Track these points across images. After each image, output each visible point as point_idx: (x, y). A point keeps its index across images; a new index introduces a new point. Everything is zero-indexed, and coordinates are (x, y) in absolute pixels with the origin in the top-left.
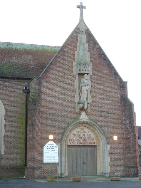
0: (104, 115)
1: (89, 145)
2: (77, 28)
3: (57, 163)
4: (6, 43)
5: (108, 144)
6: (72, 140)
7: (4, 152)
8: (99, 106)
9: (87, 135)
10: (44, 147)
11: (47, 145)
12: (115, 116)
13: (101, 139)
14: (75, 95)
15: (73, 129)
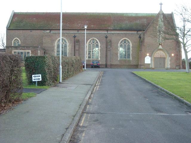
4: (135, 13)
15: (157, 51)
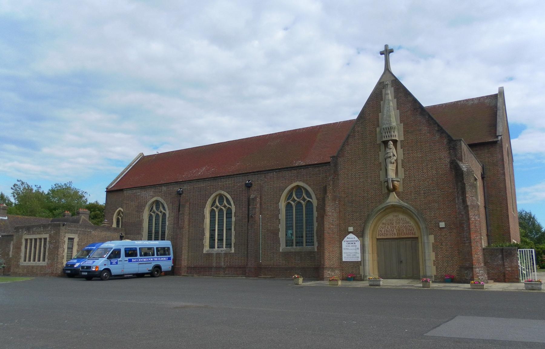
1: (406, 236)
2: (382, 81)
3: (359, 262)
6: (382, 232)
7: (317, 249)
10: (343, 242)
11: (346, 239)
12: (442, 193)
14: (381, 172)
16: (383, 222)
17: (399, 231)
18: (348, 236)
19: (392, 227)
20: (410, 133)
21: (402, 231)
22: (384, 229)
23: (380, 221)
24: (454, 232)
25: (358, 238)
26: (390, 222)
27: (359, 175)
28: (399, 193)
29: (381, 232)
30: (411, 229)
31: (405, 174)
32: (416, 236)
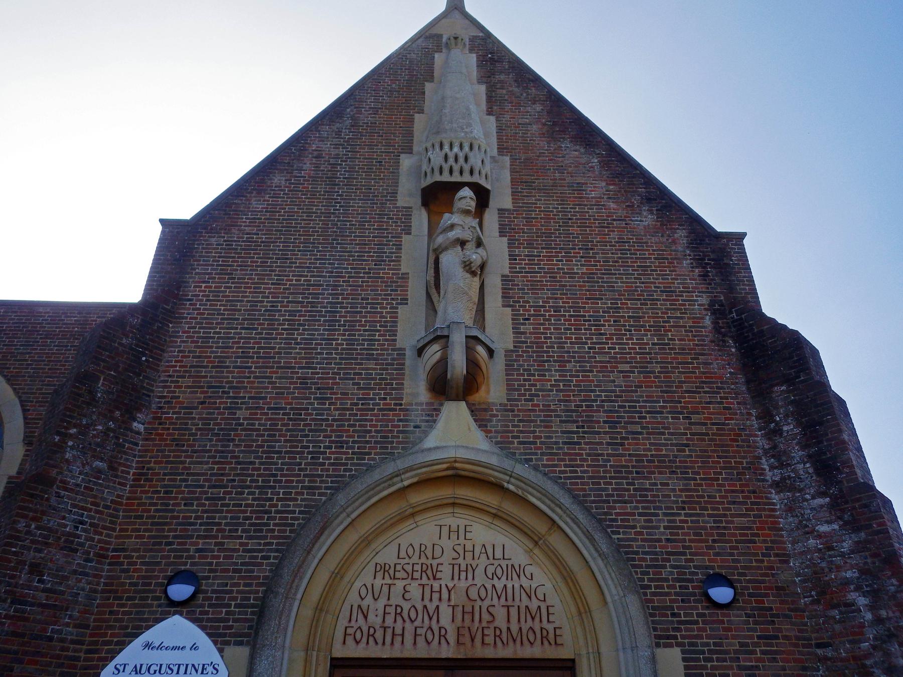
0: (613, 424)
2: (435, 31)
5: (662, 639)
6: (371, 617)
8: (569, 366)
9: (491, 570)
13: (605, 603)
16: (379, 559)
17: (468, 617)
18: (152, 635)
19: (427, 590)
20: (538, 189)
21: (486, 617)
22: (382, 601)
23: (367, 553)
24: (786, 637)
25: (221, 651)
26: (423, 560)
27: (292, 313)
28: (485, 410)
29: (366, 617)
30: (534, 610)
31: (517, 332)
32: (565, 653)
